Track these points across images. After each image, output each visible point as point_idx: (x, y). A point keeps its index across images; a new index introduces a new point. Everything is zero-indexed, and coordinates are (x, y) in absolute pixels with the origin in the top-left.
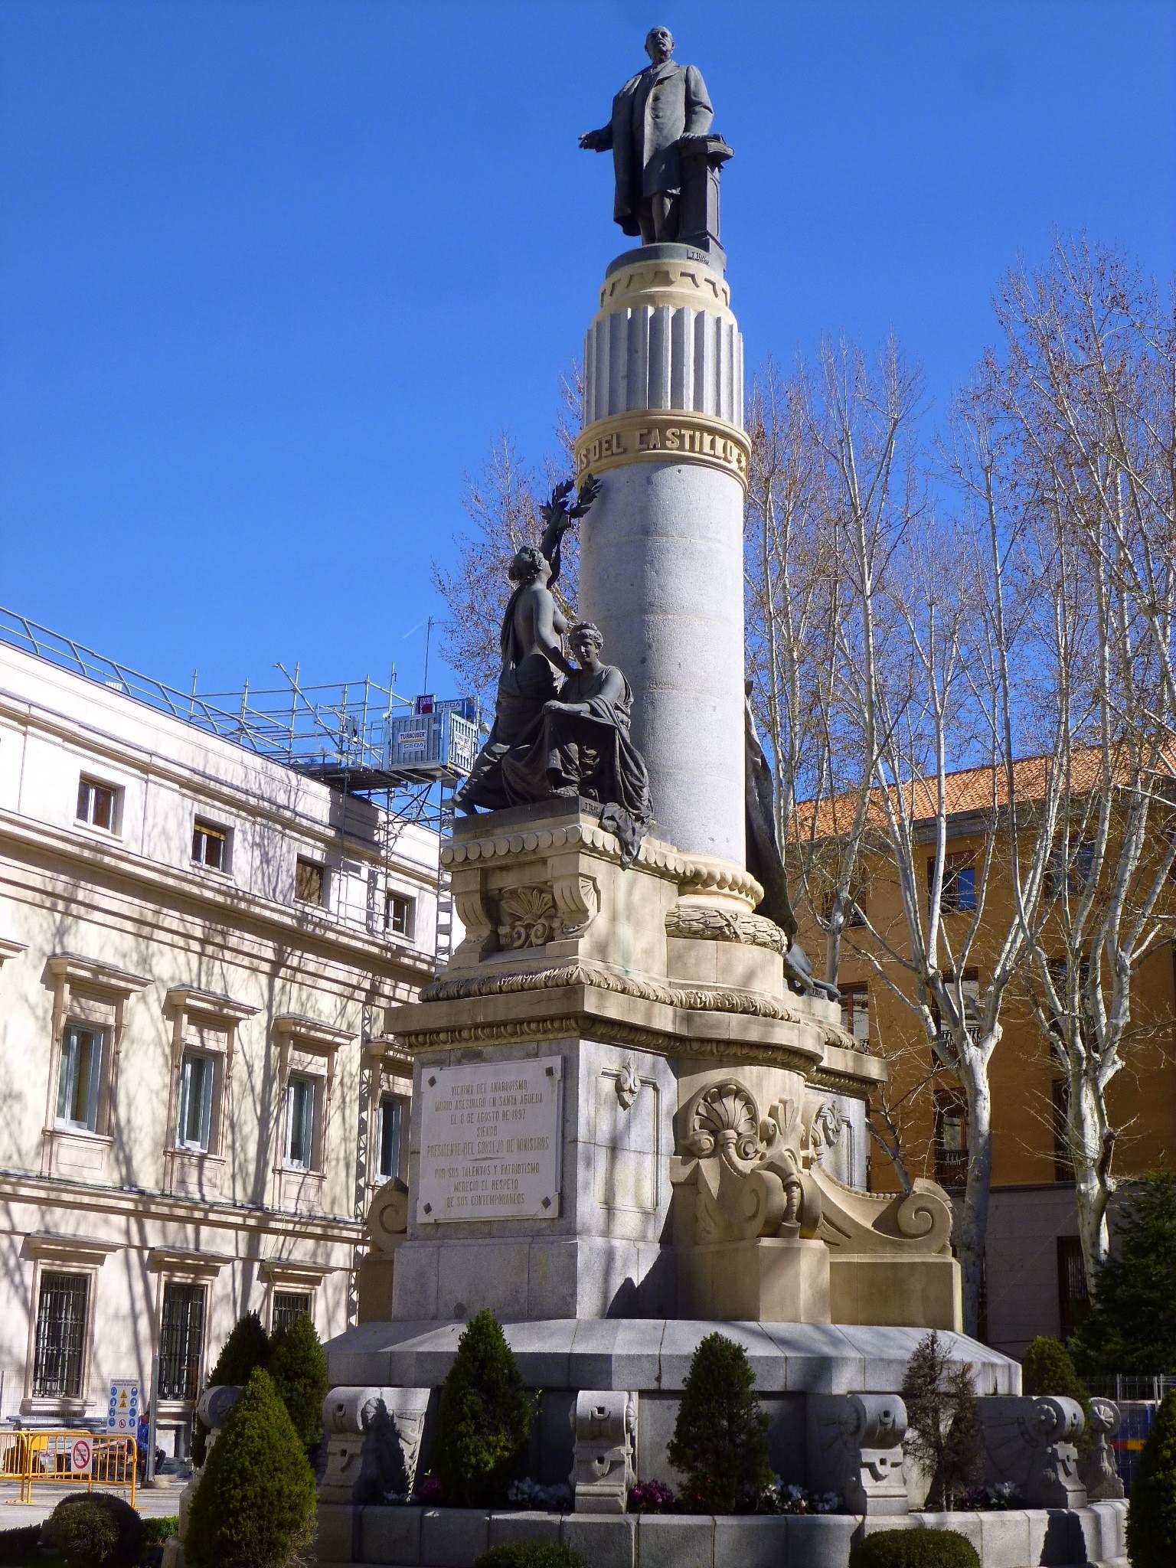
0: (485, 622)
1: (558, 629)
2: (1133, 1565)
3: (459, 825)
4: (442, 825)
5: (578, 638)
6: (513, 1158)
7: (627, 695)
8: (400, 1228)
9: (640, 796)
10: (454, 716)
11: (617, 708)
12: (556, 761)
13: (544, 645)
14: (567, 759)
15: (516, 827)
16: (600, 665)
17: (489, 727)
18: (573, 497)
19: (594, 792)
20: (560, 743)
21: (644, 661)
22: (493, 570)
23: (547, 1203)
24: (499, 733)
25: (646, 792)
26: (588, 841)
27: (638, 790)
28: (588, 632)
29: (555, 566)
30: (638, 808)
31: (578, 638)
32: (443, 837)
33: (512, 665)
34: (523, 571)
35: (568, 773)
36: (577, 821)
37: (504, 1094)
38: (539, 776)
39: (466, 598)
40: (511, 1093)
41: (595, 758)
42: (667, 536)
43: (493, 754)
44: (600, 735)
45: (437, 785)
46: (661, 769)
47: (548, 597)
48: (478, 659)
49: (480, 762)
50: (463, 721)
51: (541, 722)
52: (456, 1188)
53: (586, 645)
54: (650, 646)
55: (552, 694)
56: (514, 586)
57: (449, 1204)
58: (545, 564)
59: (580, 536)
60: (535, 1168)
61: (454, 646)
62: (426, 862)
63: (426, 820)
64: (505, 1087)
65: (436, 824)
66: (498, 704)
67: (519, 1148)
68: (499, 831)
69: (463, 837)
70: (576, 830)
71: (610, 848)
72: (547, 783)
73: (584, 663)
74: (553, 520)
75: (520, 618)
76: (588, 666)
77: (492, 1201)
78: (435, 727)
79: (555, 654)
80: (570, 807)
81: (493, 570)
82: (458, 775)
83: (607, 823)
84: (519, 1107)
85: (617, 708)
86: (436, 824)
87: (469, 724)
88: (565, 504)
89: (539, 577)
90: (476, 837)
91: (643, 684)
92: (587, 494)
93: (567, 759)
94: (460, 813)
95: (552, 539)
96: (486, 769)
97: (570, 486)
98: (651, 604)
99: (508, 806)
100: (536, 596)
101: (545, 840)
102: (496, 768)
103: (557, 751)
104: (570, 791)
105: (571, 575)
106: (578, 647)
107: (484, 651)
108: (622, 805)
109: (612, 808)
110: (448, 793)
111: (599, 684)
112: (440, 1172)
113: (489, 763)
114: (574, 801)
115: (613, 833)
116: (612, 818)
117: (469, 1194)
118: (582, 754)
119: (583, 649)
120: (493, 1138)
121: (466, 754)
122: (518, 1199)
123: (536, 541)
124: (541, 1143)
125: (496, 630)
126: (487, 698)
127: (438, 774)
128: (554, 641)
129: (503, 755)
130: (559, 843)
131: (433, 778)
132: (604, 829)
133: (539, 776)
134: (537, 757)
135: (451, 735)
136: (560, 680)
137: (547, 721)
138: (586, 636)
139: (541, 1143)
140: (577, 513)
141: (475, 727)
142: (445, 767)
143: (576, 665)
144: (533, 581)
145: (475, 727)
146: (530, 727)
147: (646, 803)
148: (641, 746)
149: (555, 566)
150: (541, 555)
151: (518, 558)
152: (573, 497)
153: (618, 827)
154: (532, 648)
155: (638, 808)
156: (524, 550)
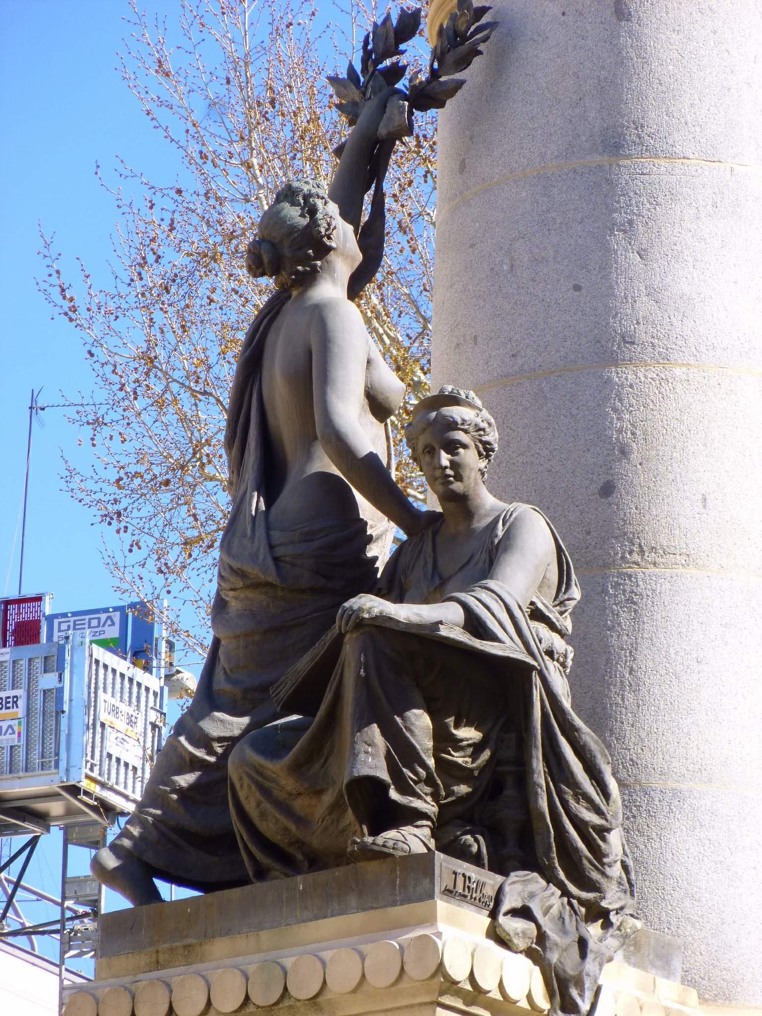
0: (185, 398)
1: (379, 407)
3: (113, 933)
4: (65, 946)
5: (433, 431)
7: (564, 581)
9: (598, 854)
10: (100, 653)
11: (537, 615)
12: (371, 757)
13: (341, 448)
14: (402, 751)
15: (266, 937)
16: (488, 501)
17: (191, 679)
18: (418, 54)
19: (475, 843)
20: (383, 711)
21: (607, 490)
22: (207, 258)
24: (220, 683)
25: (615, 842)
26: (458, 971)
27: (594, 837)
28: (456, 412)
29: (372, 240)
30: (592, 886)
31: (433, 431)
32: (70, 979)
33: (256, 503)
34: (287, 253)
35: (405, 789)
36: (430, 919)
38: (328, 798)
39: (131, 336)
41: (477, 748)
42: (671, 157)
43: (204, 741)
44: (491, 688)
45: (51, 841)
46: (656, 782)
47: (350, 326)
48: (165, 497)
49: (169, 761)
50: (123, 665)
51: (331, 659)
53: (452, 447)
54: (624, 452)
55: (363, 578)
56: (260, 291)
58: (344, 236)
59: (440, 164)
61: (101, 459)
62: (39, 936)
63: (23, 932)
65: (48, 945)
66: (220, 606)
68: (219, 947)
69: (122, 962)
70: (427, 945)
71: (517, 993)
72: (350, 816)
73: (451, 498)
74: (367, 111)
75: (271, 411)
76: (459, 504)
78: (48, 681)
79: (372, 474)
80: (411, 881)
81: (207, 258)
82: (107, 810)
83: (512, 925)
85: (537, 615)
86: (48, 945)
87: (139, 675)
88: (397, 72)
89: (329, 268)
90: (158, 965)
91: (603, 555)
92: (456, 47)
93: (402, 751)
94: (113, 901)
95: (365, 165)
96: (185, 780)
97: (408, 25)
98: (628, 340)
99: (243, 881)
100: (319, 316)
101: (343, 972)
102: (214, 783)
103: (375, 729)
104: (414, 839)
105: (415, 270)
106: (431, 451)
107: (175, 476)
108: (550, 878)
109: (521, 887)
110: (81, 861)
111: (487, 554)
113: (194, 764)
114: (421, 866)
115: (530, 953)
116: (524, 913)
118: (444, 740)
119: (445, 459)
121: (133, 754)
123: (320, 177)
125: (214, 419)
126: (189, 612)
127: (55, 808)
128: (367, 436)
129: (232, 741)
130: (380, 979)
131: (42, 819)
132: (503, 942)
133: (328, 798)
134: (323, 746)
135: (91, 704)
136: (384, 539)
137: (350, 651)
138: (453, 425)
140: (427, 97)
141: (153, 681)
142: (74, 790)
143: (425, 499)
144: (309, 279)
145: (153, 681)
146: (305, 663)
147: (616, 871)
148: (601, 719)
149: (372, 240)
150: (333, 209)
151: (272, 218)
152: (418, 54)
153: (542, 937)
154: (308, 456)
155: (592, 886)
156: (288, 194)
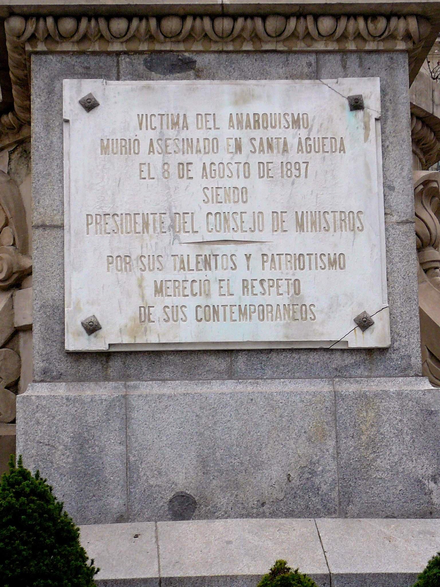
2: (1, 103)
6: (292, 242)
8: (11, 419)
23: (364, 323)
37: (257, 134)
40: (272, 133)
52: (159, 290)
57: (144, 316)
60: (336, 262)
64: (258, 122)
67: (300, 226)
77: (243, 313)
84: (294, 156)
97: (73, 42)
112: (122, 261)
117: (191, 303)
120: (240, 207)
122: (299, 310)
124: (350, 221)
139: (350, 221)
